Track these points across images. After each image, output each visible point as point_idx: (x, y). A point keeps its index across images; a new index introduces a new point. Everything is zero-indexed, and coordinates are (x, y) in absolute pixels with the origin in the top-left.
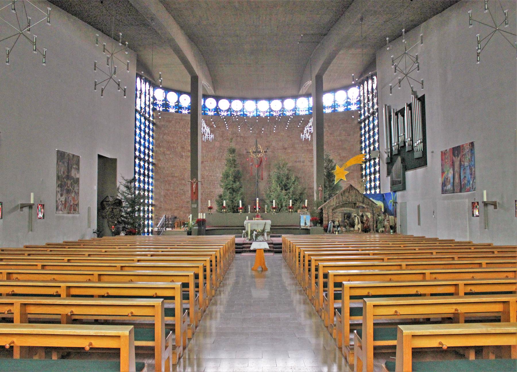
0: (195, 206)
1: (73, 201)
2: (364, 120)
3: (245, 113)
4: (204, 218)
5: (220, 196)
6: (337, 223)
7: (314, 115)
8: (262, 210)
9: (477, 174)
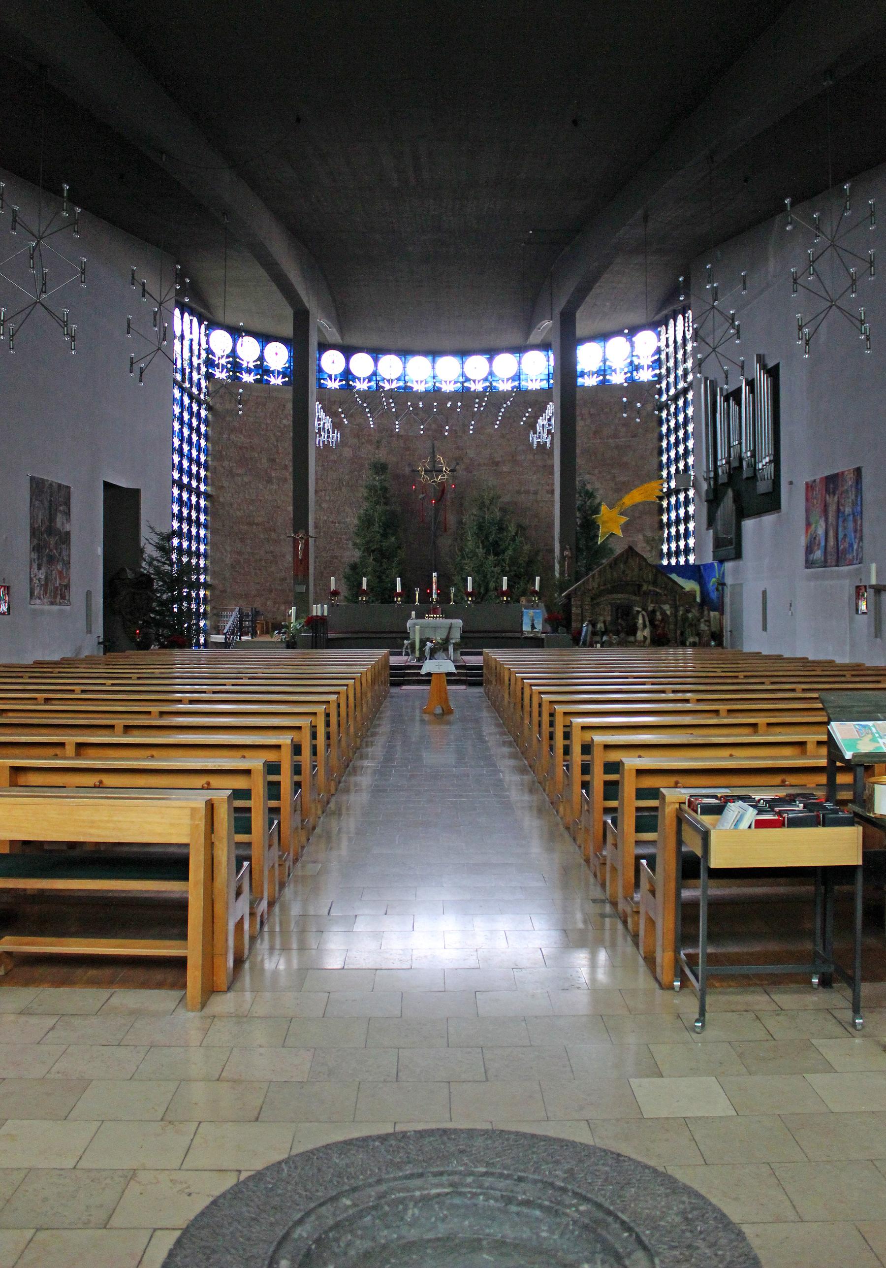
0: (303, 588)
1: (60, 579)
2: (675, 398)
3: (409, 384)
4: (326, 614)
5: (354, 567)
6: (600, 626)
7: (557, 394)
9: (866, 530)
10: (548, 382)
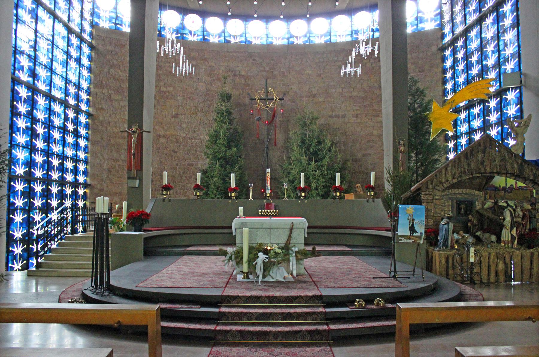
8: (277, 194)
10: (352, 36)
